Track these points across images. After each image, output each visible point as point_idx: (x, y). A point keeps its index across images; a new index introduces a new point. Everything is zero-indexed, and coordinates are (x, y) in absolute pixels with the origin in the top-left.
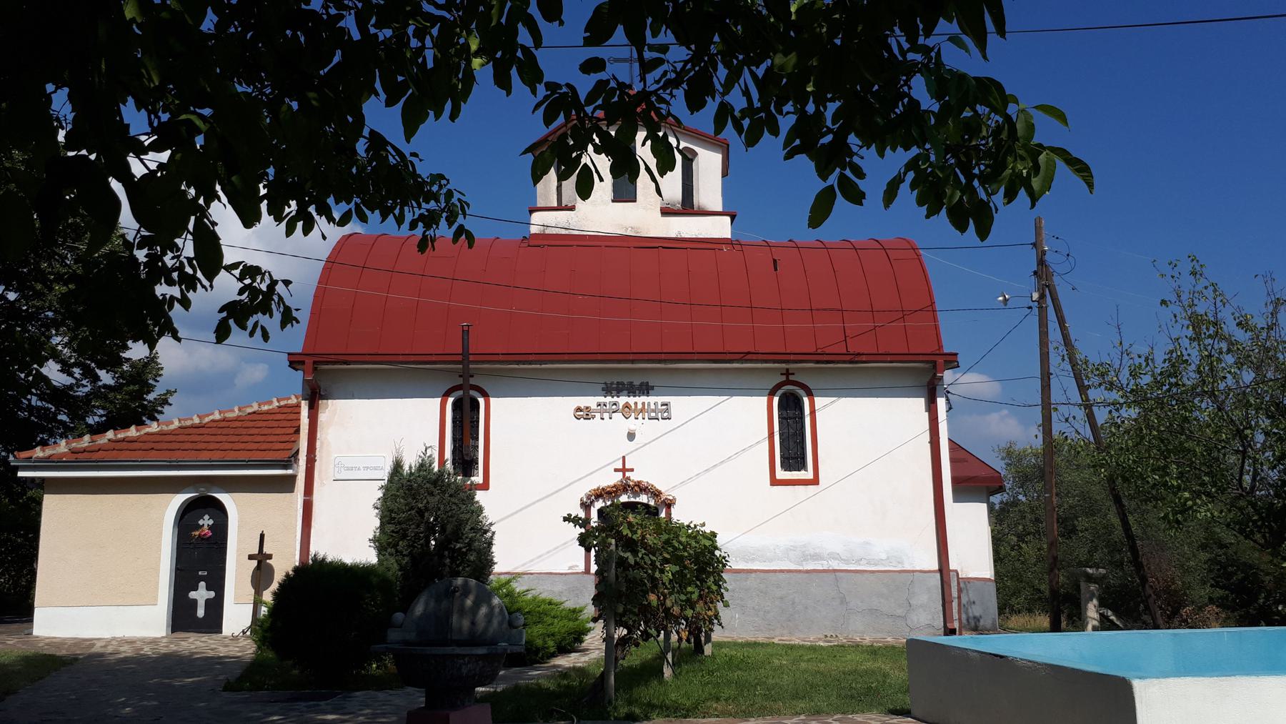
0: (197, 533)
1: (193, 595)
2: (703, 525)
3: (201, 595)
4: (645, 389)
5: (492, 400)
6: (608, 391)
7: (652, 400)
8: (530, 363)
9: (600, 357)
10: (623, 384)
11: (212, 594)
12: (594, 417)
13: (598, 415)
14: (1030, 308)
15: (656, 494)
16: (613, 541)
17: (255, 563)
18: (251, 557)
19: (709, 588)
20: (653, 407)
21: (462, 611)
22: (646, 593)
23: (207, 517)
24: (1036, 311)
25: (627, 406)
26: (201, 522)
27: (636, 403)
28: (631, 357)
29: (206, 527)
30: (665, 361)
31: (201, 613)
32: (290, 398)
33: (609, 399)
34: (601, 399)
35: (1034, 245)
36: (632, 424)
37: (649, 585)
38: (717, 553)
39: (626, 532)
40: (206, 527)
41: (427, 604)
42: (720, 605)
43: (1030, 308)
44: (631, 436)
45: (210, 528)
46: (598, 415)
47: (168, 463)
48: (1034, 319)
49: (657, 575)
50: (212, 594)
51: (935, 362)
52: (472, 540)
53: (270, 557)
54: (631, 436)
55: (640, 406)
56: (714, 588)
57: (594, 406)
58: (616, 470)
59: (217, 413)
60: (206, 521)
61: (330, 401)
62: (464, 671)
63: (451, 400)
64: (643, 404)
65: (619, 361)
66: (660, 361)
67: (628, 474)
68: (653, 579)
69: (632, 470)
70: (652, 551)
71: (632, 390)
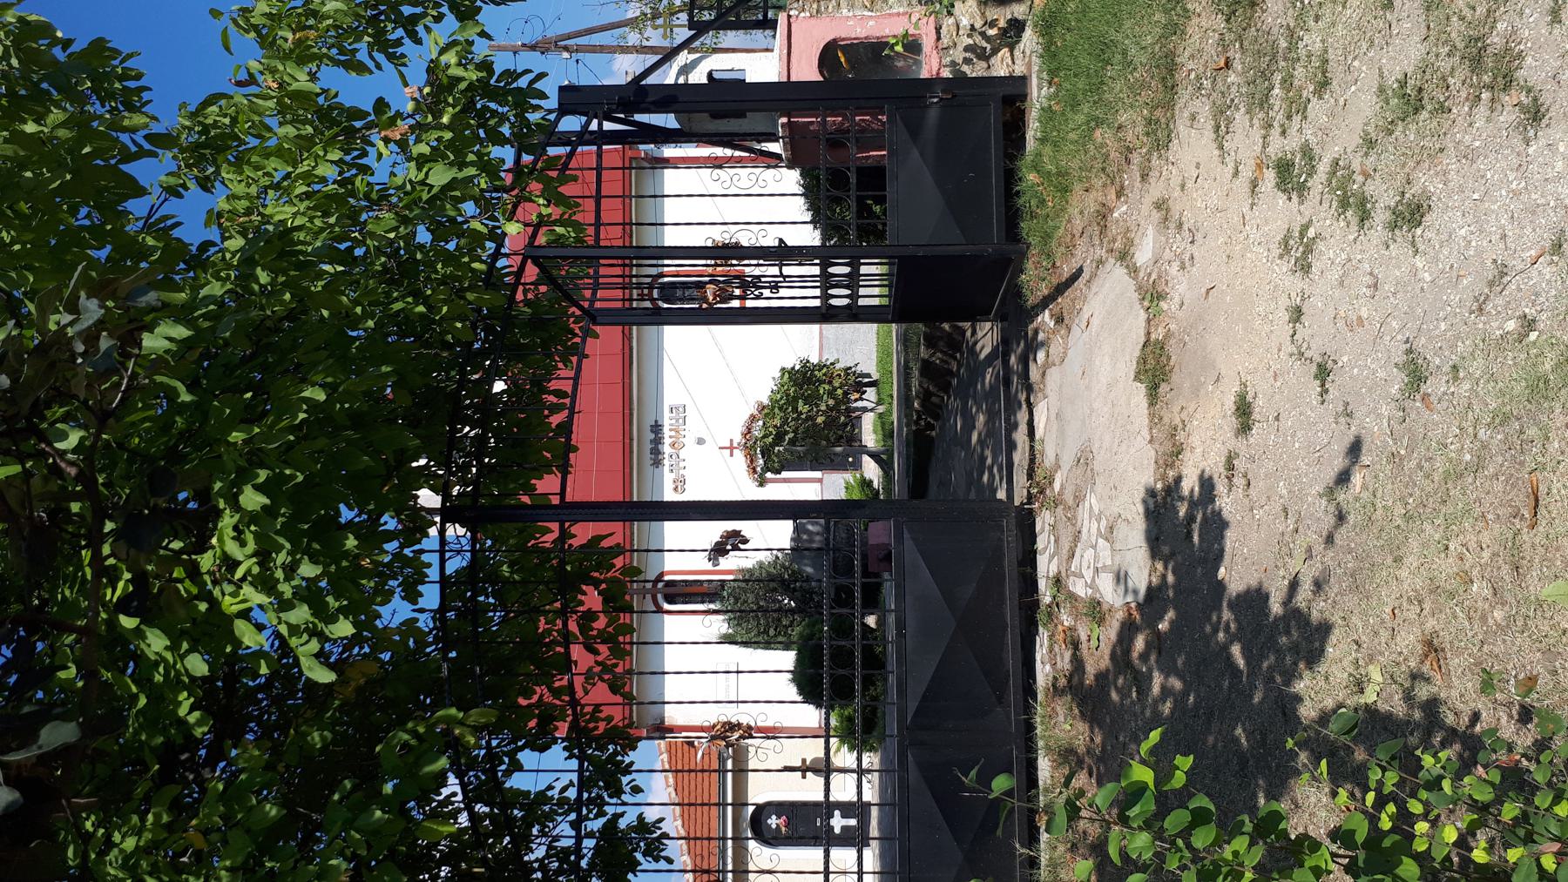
0: (783, 829)
1: (837, 830)
2: (774, 378)
3: (838, 822)
4: (657, 428)
5: (666, 569)
6: (657, 463)
7: (667, 422)
8: (632, 534)
9: (627, 470)
10: (652, 449)
11: (837, 813)
12: (683, 476)
13: (682, 472)
14: (577, 61)
15: (753, 418)
16: (777, 448)
17: (809, 774)
18: (804, 777)
19: (824, 375)
20: (674, 421)
21: (811, 541)
22: (815, 425)
23: (769, 821)
24: (580, 56)
25: (673, 445)
26: (774, 826)
27: (670, 437)
28: (627, 441)
29: (778, 822)
30: (631, 410)
31: (853, 822)
32: (662, 760)
33: (666, 462)
34: (666, 469)
35: (515, 53)
36: (690, 441)
37: (810, 423)
38: (797, 368)
39: (770, 439)
40: (778, 822)
41: (806, 565)
42: (838, 366)
43: (577, 61)
44: (701, 441)
45: (779, 817)
46: (682, 472)
47: (660, 262)
48: (588, 58)
49: (803, 416)
50: (837, 813)
51: (631, 158)
52: (783, 566)
53: (804, 761)
54: (701, 441)
55: (673, 433)
56: (825, 370)
57: (673, 476)
58: (732, 455)
59: (676, 823)
60: (773, 821)
61: (666, 715)
62: (844, 535)
63: (667, 606)
64: (671, 430)
65: (631, 452)
66: (631, 414)
67: (735, 445)
68: (807, 419)
69: (731, 441)
70: (785, 422)
71: (658, 441)
